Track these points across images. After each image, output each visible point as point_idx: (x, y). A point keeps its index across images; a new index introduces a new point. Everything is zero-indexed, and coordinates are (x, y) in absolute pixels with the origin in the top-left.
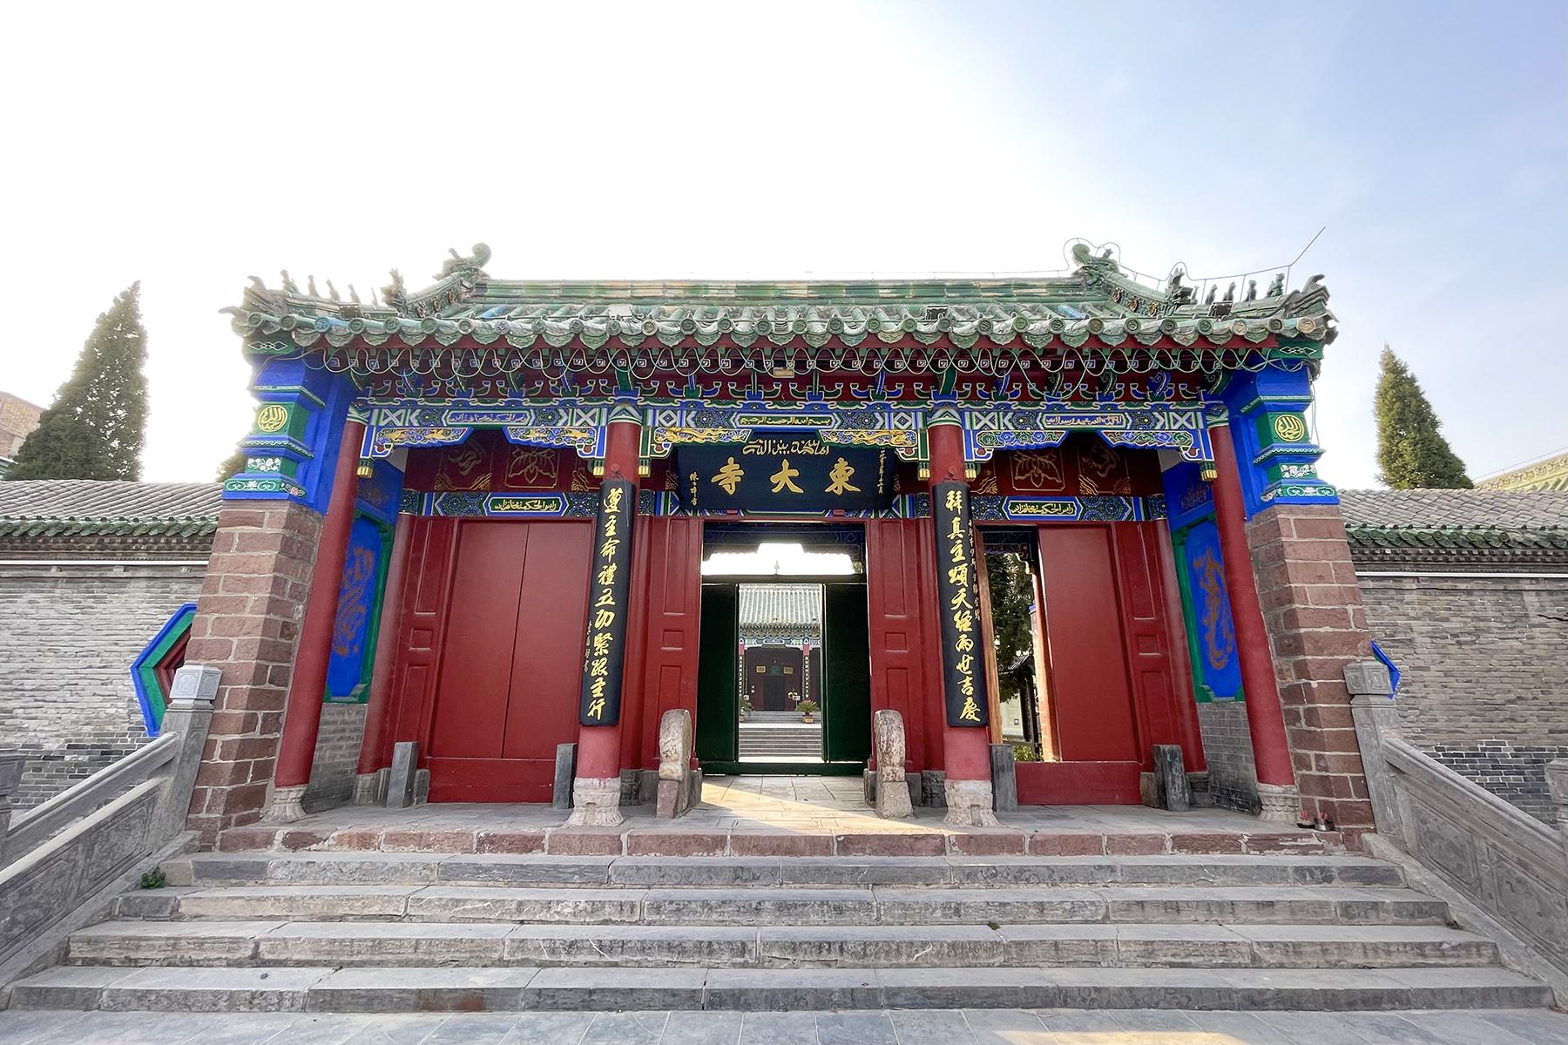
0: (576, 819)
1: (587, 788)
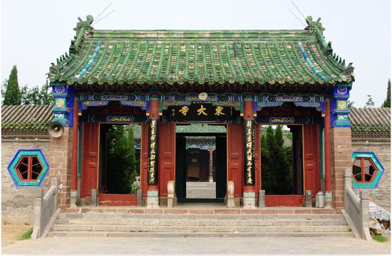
0: (149, 207)
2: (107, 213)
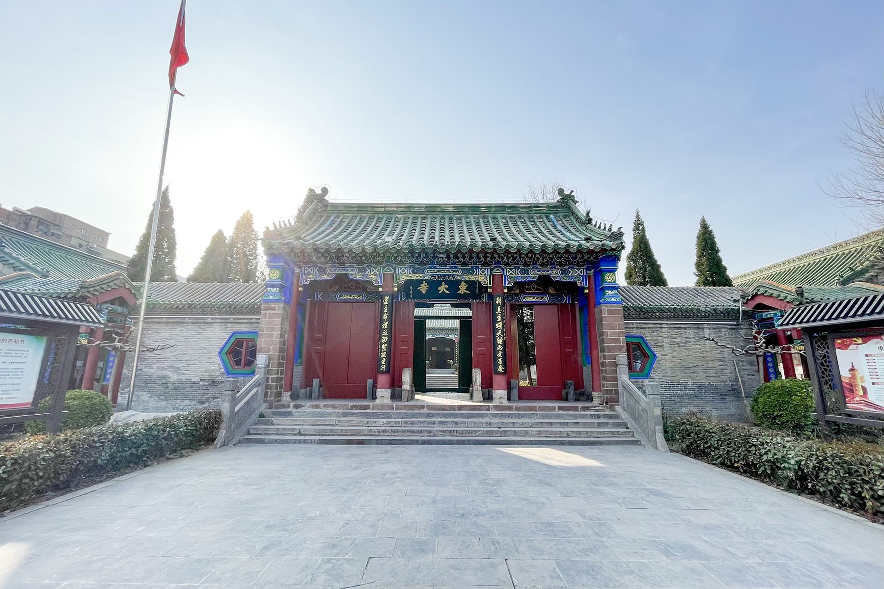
0: (378, 401)
1: (380, 392)
2: (324, 410)
